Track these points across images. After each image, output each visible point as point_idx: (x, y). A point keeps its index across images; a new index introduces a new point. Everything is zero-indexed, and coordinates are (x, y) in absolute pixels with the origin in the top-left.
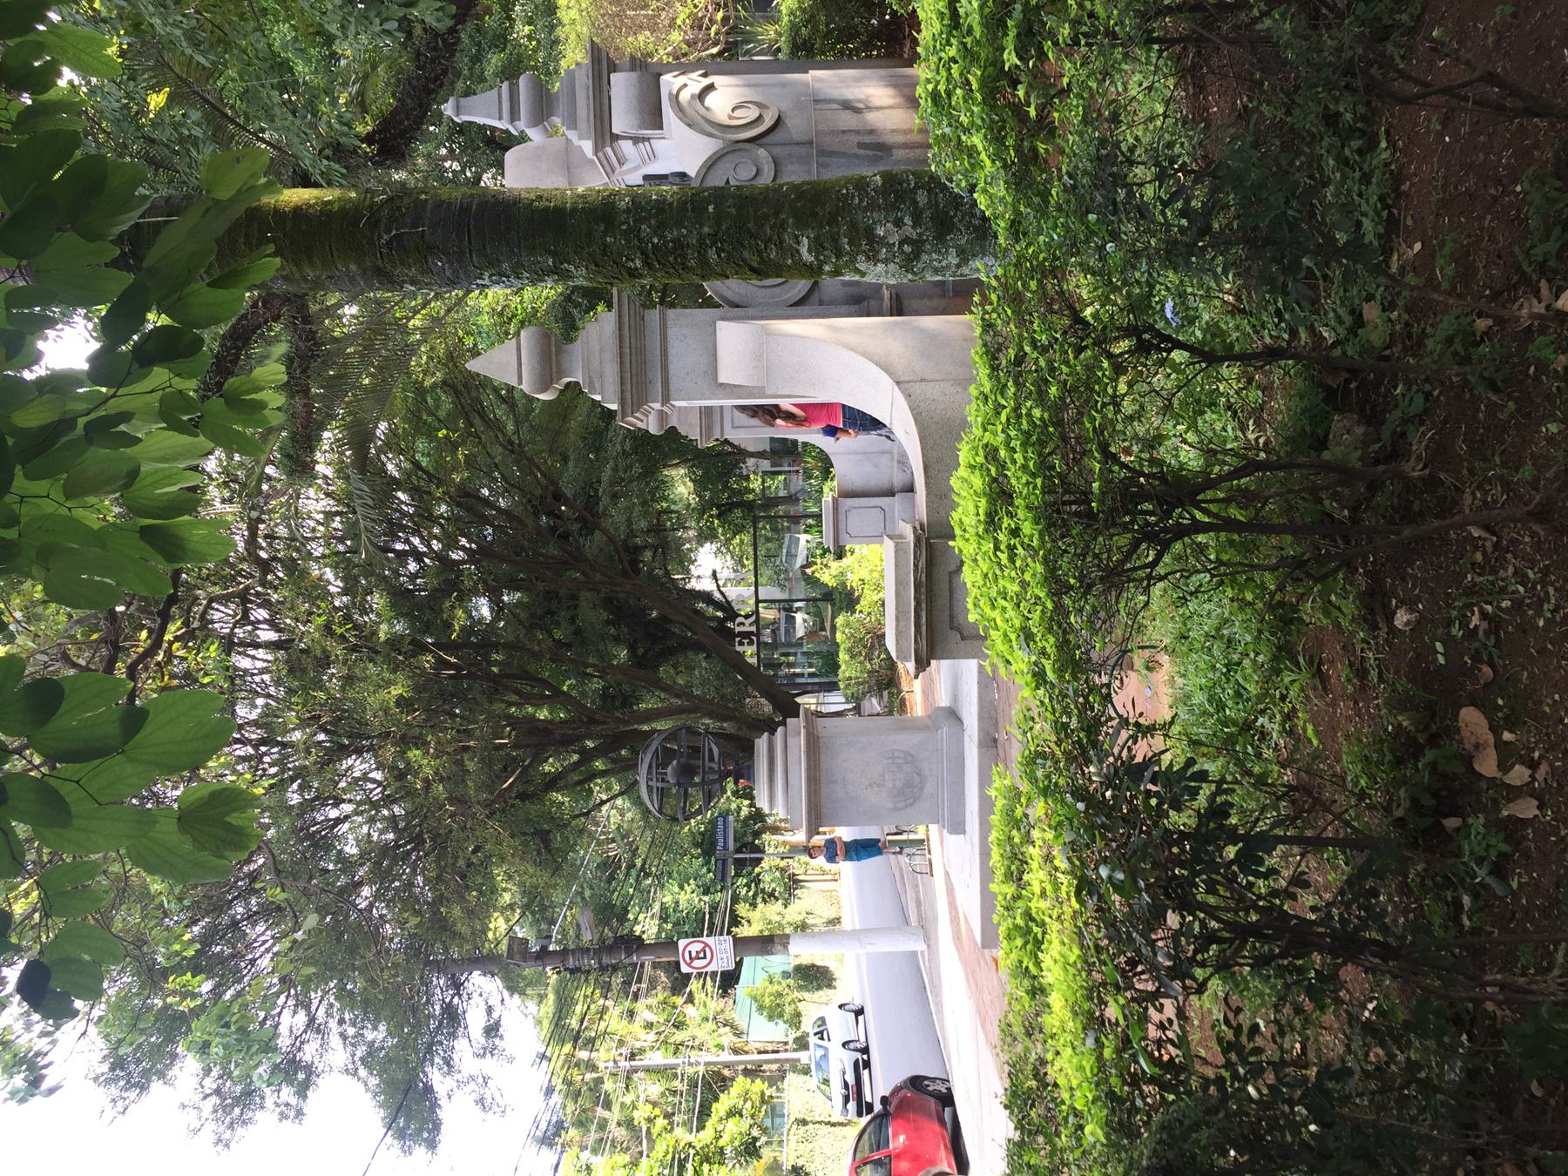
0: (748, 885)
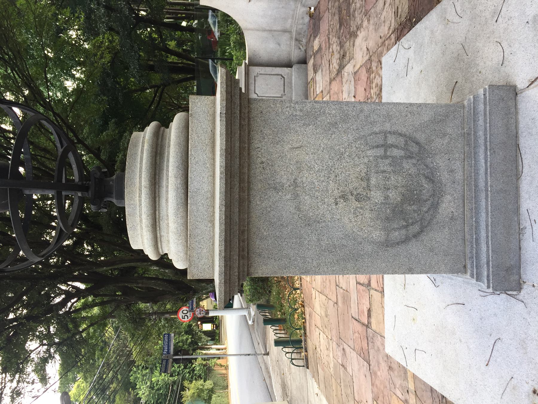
0: (189, 372)
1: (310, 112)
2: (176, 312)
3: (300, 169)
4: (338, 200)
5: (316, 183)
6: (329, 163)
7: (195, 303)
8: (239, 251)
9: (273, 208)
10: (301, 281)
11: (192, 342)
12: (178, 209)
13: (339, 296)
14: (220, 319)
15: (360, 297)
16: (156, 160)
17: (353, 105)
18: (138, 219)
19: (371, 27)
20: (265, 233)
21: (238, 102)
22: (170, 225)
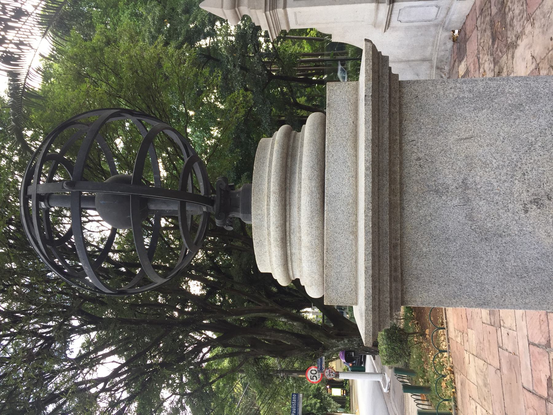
1: (484, 92)
2: (304, 372)
3: (470, 166)
4: (528, 206)
5: (495, 184)
6: (513, 157)
7: (324, 363)
8: (391, 271)
9: (436, 217)
10: (449, 342)
11: (320, 407)
12: (312, 218)
13: (502, 361)
14: (350, 385)
15: (534, 362)
16: (286, 162)
17: (545, 80)
18: (266, 232)
19: (537, 31)
20: (424, 250)
21: (386, 83)
22: (303, 238)
